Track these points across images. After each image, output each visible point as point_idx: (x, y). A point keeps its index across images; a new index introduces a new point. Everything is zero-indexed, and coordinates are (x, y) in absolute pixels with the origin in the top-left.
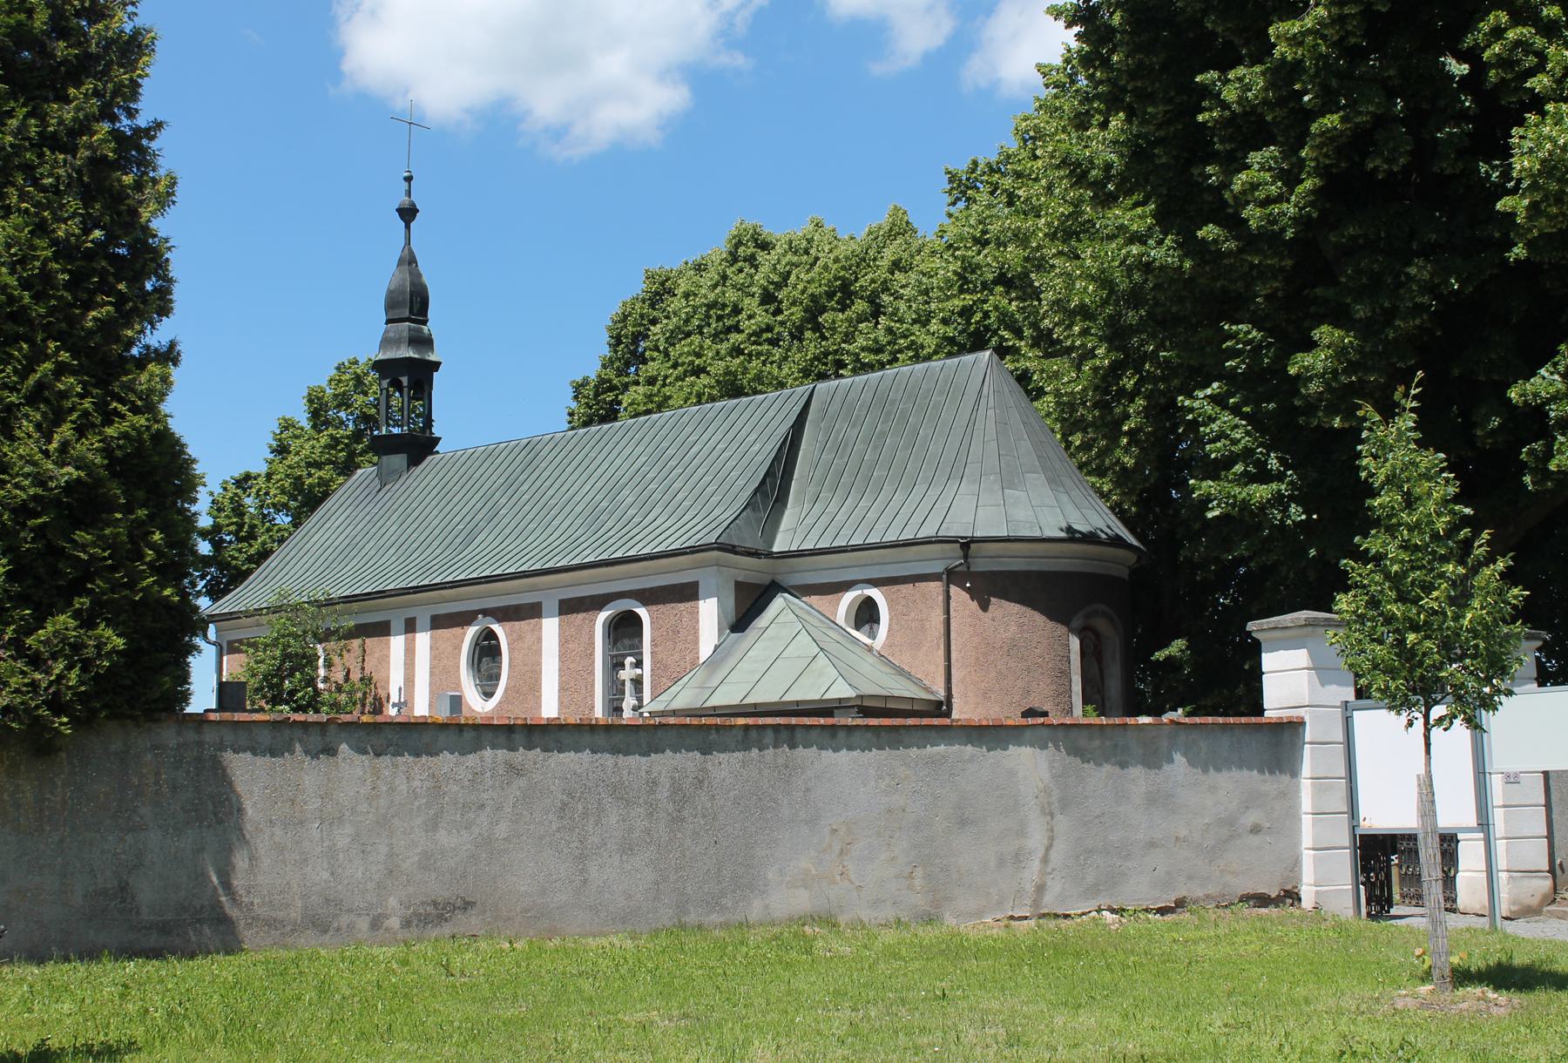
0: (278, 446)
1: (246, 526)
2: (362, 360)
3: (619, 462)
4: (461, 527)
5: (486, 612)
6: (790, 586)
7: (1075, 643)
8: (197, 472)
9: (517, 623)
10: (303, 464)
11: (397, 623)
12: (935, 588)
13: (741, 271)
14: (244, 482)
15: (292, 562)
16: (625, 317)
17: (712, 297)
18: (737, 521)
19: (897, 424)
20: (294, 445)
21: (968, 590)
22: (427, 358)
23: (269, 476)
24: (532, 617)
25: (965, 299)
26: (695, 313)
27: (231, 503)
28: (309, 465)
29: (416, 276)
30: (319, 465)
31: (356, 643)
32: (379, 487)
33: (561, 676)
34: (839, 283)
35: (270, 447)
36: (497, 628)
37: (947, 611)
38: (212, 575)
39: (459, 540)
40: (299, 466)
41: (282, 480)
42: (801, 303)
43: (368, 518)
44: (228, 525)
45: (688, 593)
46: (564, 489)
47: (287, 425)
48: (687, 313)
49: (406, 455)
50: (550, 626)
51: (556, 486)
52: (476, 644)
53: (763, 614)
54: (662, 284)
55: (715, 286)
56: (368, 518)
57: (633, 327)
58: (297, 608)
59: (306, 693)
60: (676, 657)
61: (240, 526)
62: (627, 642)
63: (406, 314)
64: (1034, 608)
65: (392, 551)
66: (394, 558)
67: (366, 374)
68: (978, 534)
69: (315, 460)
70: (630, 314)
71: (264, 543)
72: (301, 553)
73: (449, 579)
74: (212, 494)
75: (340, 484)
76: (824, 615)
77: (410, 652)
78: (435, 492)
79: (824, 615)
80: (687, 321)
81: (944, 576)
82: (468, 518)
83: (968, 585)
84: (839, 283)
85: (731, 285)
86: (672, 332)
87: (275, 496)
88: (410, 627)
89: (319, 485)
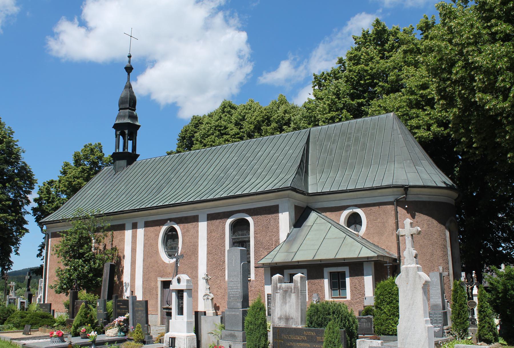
0: (63, 171)
1: (51, 198)
2: (93, 144)
3: (223, 160)
4: (154, 186)
5: (171, 220)
6: (315, 208)
7: (448, 233)
8: (35, 179)
9: (186, 224)
10: (72, 177)
11: (129, 225)
12: (390, 208)
13: (226, 116)
14: (51, 183)
15: (79, 201)
16: (186, 131)
17: (217, 123)
18: (295, 179)
19: (354, 142)
20: (69, 171)
21: (406, 209)
22: (135, 123)
23: (60, 181)
24: (194, 222)
25: (332, 114)
26: (211, 129)
27: (46, 190)
28: (74, 177)
29: (132, 93)
30: (78, 178)
31: (110, 233)
32: (114, 173)
33: (208, 248)
34: (266, 117)
35: (61, 171)
36: (176, 227)
37: (397, 218)
38: (38, 215)
39: (154, 191)
40: (71, 178)
41: (64, 182)
42: (254, 123)
43: (111, 184)
44: (45, 197)
45: (274, 210)
46: (201, 170)
47: (67, 165)
48: (208, 129)
49: (126, 161)
50: (203, 226)
51: (196, 169)
52: (166, 234)
53: (308, 220)
54: (199, 121)
55: (217, 121)
56: (111, 184)
57: (189, 134)
58: (86, 218)
59: (89, 254)
60: (267, 238)
61: (49, 198)
62: (240, 233)
63: (128, 106)
64: (433, 218)
65: (124, 196)
66: (125, 199)
67: (94, 149)
68: (411, 184)
69: (76, 176)
70: (188, 130)
71: (57, 204)
72: (83, 198)
73: (155, 205)
74: (39, 187)
75: (85, 184)
76: (333, 221)
77: (134, 237)
78: (140, 174)
79: (333, 221)
80: (208, 131)
81: (395, 203)
82: (157, 183)
83: (406, 207)
84: (266, 117)
85: (223, 120)
86: (203, 135)
87: (62, 187)
88: (135, 226)
89: (78, 184)
